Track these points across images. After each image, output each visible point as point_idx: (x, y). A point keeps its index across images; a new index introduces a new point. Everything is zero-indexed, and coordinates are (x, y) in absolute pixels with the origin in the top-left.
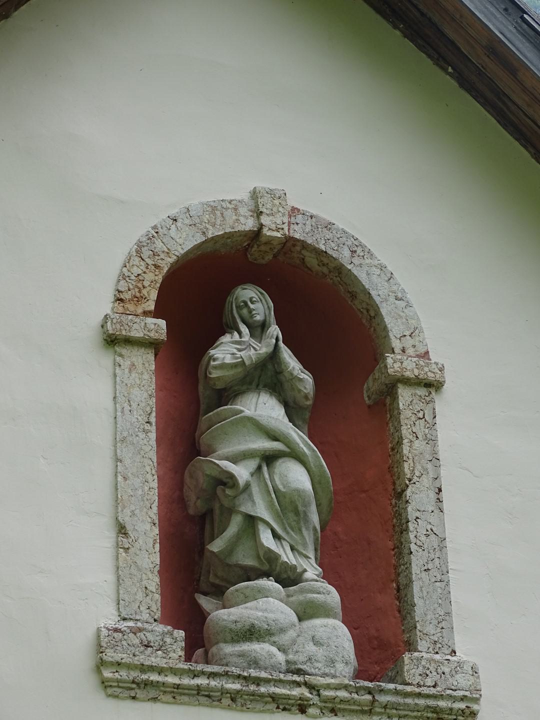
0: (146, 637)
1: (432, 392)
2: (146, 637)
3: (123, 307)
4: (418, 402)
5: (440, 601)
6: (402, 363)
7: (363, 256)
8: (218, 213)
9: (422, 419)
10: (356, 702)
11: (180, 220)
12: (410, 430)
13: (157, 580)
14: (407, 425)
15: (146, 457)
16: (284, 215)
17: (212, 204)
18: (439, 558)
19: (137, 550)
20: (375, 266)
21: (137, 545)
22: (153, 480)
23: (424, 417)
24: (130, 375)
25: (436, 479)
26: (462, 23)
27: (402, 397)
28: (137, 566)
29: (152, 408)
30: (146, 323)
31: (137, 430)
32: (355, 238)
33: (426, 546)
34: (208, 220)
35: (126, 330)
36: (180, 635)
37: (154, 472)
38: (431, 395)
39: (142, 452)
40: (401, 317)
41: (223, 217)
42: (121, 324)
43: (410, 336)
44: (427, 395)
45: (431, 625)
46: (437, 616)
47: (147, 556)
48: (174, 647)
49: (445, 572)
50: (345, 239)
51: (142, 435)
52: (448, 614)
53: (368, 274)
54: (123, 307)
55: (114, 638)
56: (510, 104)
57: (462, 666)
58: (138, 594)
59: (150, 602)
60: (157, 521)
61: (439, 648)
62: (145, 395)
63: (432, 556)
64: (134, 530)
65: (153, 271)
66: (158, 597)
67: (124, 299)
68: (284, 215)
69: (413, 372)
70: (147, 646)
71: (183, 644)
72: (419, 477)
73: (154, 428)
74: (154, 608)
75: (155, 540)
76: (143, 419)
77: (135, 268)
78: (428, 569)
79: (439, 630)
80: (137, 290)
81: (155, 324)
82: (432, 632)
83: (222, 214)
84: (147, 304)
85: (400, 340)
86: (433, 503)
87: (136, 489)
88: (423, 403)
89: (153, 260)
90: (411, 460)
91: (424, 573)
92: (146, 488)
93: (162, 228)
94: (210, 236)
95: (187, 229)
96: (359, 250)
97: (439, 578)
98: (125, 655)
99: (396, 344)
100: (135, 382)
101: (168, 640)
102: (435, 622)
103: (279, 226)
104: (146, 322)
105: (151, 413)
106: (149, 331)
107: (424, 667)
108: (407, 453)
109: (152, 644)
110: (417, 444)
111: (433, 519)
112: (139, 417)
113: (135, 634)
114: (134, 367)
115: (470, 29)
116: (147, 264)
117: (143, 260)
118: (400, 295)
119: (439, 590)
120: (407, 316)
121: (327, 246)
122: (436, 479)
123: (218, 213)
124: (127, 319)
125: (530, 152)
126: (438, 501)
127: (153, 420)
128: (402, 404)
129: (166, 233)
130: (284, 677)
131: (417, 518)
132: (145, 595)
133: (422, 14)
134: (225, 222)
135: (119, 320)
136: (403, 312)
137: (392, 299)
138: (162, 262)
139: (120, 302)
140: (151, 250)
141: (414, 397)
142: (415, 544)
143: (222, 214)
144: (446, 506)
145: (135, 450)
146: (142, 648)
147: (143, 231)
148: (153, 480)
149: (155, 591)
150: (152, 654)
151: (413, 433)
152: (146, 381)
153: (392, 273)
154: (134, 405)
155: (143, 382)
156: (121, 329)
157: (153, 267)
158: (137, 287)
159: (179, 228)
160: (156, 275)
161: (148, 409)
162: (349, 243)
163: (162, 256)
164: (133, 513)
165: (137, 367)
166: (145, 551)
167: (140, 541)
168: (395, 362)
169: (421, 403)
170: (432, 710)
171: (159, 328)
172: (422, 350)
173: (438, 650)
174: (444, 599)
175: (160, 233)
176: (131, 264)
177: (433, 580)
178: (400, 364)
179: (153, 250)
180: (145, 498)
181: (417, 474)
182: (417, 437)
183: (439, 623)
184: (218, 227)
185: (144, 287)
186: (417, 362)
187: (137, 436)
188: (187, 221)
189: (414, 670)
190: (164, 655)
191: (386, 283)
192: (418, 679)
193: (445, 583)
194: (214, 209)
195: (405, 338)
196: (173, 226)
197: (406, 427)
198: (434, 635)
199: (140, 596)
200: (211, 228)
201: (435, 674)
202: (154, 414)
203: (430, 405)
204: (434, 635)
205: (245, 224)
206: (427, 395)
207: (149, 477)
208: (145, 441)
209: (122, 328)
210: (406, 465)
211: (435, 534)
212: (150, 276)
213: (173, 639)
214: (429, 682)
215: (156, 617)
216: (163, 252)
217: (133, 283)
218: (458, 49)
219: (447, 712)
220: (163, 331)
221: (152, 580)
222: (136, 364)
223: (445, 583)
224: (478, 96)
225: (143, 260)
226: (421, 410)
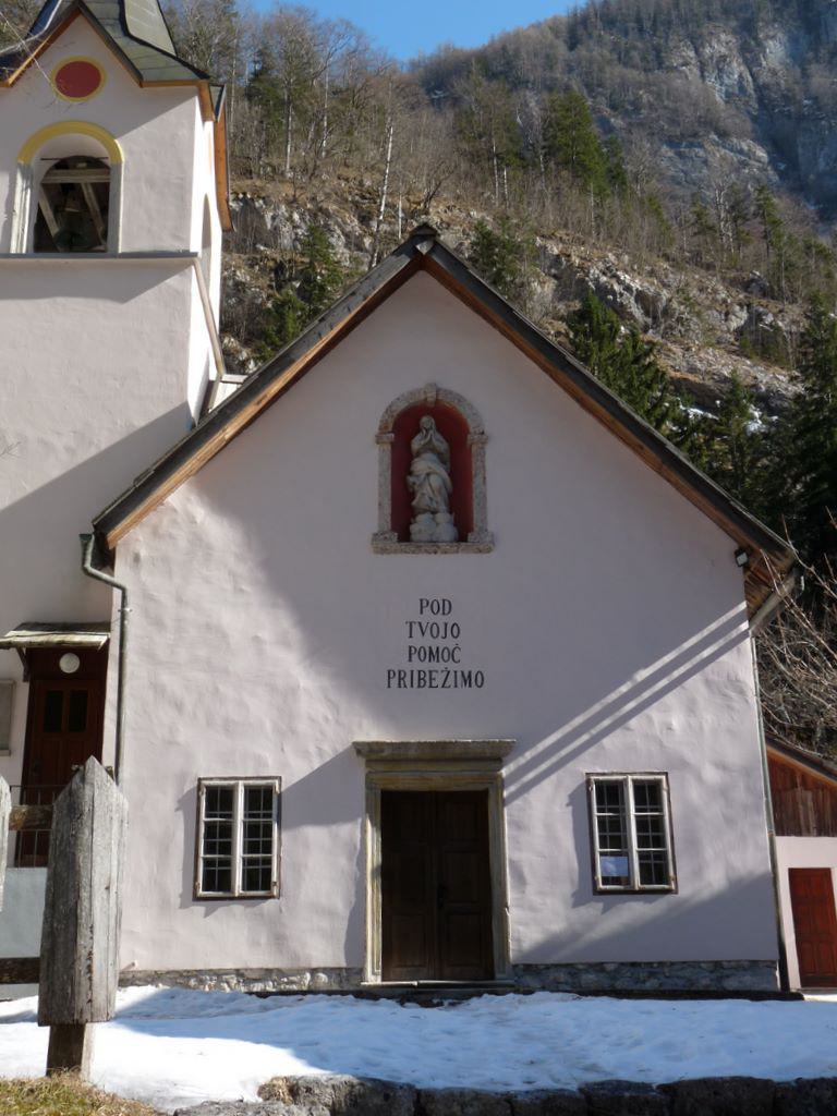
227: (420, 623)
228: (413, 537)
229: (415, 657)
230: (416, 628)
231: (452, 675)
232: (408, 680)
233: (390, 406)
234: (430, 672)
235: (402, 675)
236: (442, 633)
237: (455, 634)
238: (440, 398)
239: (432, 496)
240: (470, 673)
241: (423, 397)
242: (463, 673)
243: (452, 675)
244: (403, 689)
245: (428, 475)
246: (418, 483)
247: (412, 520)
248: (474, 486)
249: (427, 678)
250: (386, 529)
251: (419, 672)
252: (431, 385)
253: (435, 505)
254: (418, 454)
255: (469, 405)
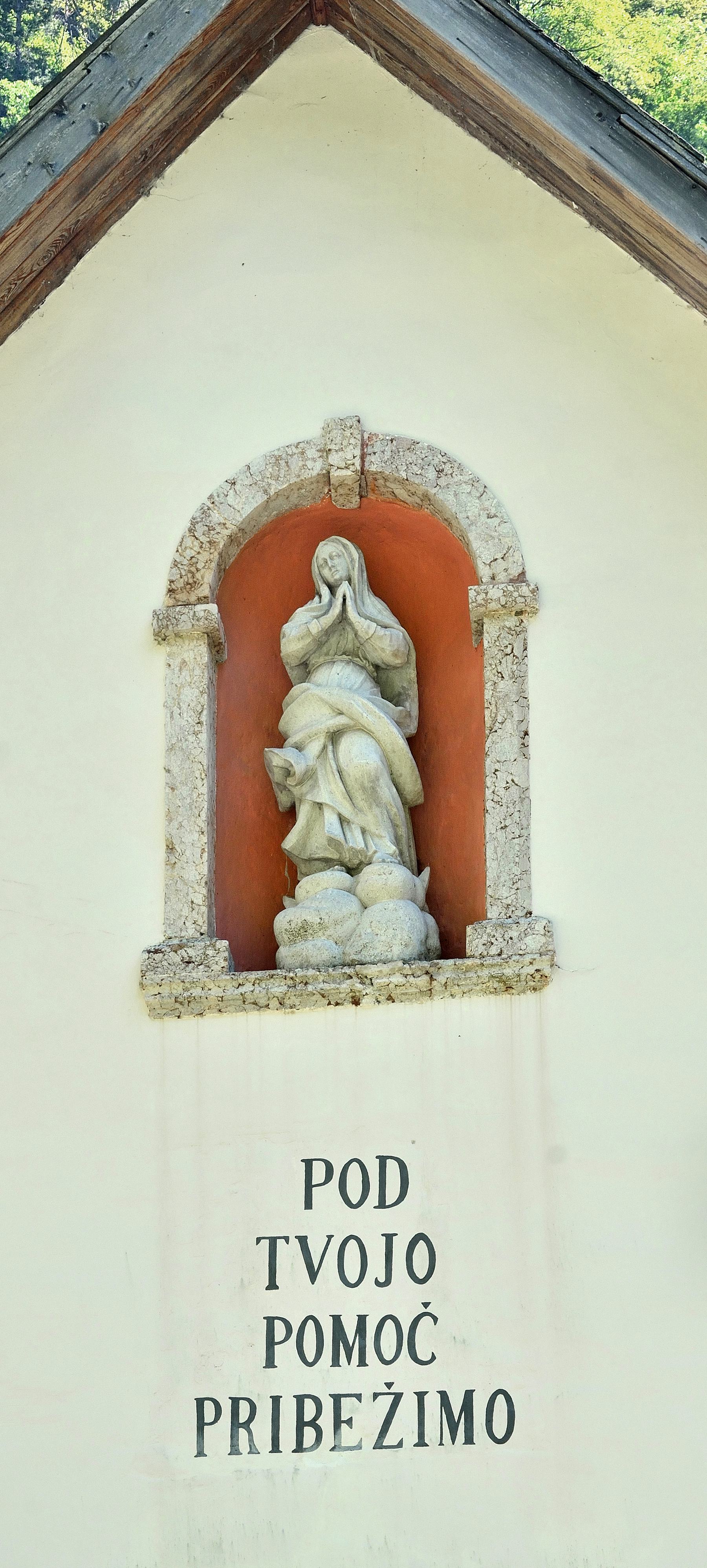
0: (188, 953)
1: (524, 620)
2: (188, 953)
3: (175, 598)
4: (507, 635)
5: (517, 860)
6: (486, 593)
7: (451, 474)
8: (282, 463)
9: (509, 655)
10: (412, 985)
11: (239, 482)
12: (494, 671)
13: (204, 891)
14: (491, 665)
15: (195, 761)
16: (355, 446)
17: (276, 453)
18: (519, 811)
19: (183, 863)
20: (465, 482)
21: (184, 858)
22: (203, 785)
23: (512, 652)
24: (181, 674)
25: (522, 721)
26: (559, 146)
27: (488, 633)
28: (183, 881)
29: (203, 706)
30: (195, 612)
31: (186, 733)
32: (443, 454)
33: (504, 801)
34: (271, 474)
35: (173, 624)
36: (223, 945)
37: (203, 776)
38: (523, 624)
39: (191, 757)
40: (493, 538)
41: (288, 466)
42: (167, 619)
43: (502, 558)
44: (518, 625)
45: (504, 888)
46: (512, 876)
47: (194, 868)
48: (217, 959)
49: (525, 826)
50: (430, 458)
51: (191, 738)
52: (526, 872)
53: (456, 495)
54: (175, 598)
55: (154, 960)
56: (633, 234)
57: (533, 927)
58: (183, 910)
59: (196, 916)
60: (205, 829)
61: (513, 911)
62: (196, 692)
63: (511, 810)
64: (182, 842)
65: (208, 549)
66: (204, 909)
67: (176, 589)
68: (355, 446)
69: (500, 601)
70: (189, 963)
71: (226, 954)
72: (502, 723)
73: (204, 728)
74: (200, 922)
75: (203, 849)
76: (193, 720)
77: (188, 551)
78: (506, 826)
79: (513, 891)
80: (190, 575)
81: (205, 610)
82: (505, 895)
83: (287, 463)
84: (202, 588)
85: (490, 565)
86: (516, 750)
87: (184, 798)
88: (512, 635)
89: (207, 536)
90: (493, 706)
91: (499, 833)
92: (195, 795)
93: (218, 496)
94: (272, 492)
95: (247, 490)
96: (447, 468)
97: (517, 833)
98: (166, 975)
99: (484, 572)
100: (186, 680)
101: (210, 952)
102: (510, 883)
103: (349, 462)
104: (195, 610)
105: (202, 711)
106: (198, 620)
107: (489, 935)
108: (490, 697)
109: (193, 960)
110: (502, 685)
111: (515, 769)
112: (190, 719)
113: (176, 952)
114: (185, 664)
115: (568, 152)
116: (201, 542)
117: (197, 539)
118: (493, 511)
119: (517, 848)
120: (500, 535)
121: (409, 471)
122: (522, 721)
123: (282, 463)
124: (175, 611)
125: (672, 288)
126: (523, 746)
127: (204, 718)
128: (487, 642)
129: (223, 501)
130: (333, 970)
131: (496, 770)
132: (191, 909)
133: (528, 145)
134: (290, 471)
135: (165, 616)
136: (496, 531)
137: (484, 518)
138: (218, 537)
139: (171, 593)
140: (206, 526)
141: (501, 632)
142: (492, 800)
143: (287, 463)
144: (532, 750)
145: (184, 756)
146: (183, 965)
147: (198, 505)
148: (203, 785)
149: (201, 904)
150: (194, 970)
151: (498, 673)
152: (198, 677)
153: (485, 487)
154: (184, 707)
155: (194, 679)
156: (167, 625)
157: (208, 544)
158: (190, 572)
159: (238, 493)
160: (211, 554)
161: (199, 708)
162: (436, 461)
163: (218, 529)
164: (181, 825)
165: (188, 663)
166: (192, 863)
167: (188, 853)
168: (478, 593)
169: (510, 637)
170: (498, 979)
171: (209, 614)
172: (515, 572)
173: (510, 914)
174: (521, 856)
175: (216, 503)
176: (183, 547)
177: (512, 836)
178: (484, 594)
179: (208, 524)
180: (193, 807)
181: (500, 719)
182: (502, 677)
183: (514, 883)
184: (282, 479)
185: (198, 570)
186: (505, 589)
187: (186, 740)
188: (248, 482)
189: (477, 940)
190: (206, 969)
191: (477, 501)
192: (481, 949)
193: (524, 838)
194: (278, 459)
195: (496, 562)
196: (231, 491)
197: (489, 668)
198: (507, 898)
199: (186, 911)
200: (273, 482)
201: (502, 940)
202: (205, 712)
203: (521, 636)
204: (507, 898)
205: (312, 469)
206: (518, 625)
207: (199, 783)
208: (195, 745)
209: (168, 623)
210: (487, 713)
211: (517, 785)
212: (204, 557)
213: (216, 950)
214: (494, 950)
215: (202, 931)
216: (219, 524)
217: (186, 568)
218: (569, 178)
219: (515, 979)
220: (213, 617)
221: (199, 893)
222: (187, 660)
223: (524, 838)
224: (608, 231)
225: (197, 539)
226: (510, 644)
227: (303, 1241)
228: (283, 953)
229: (286, 1352)
230: (289, 1254)
231: (408, 1408)
232: (262, 1427)
233: (205, 511)
234: (337, 1399)
235: (243, 1416)
236: (376, 1269)
237: (500, 1433)
238: (374, 465)
239: (347, 811)
240: (469, 1396)
241: (316, 468)
242: (444, 1395)
243: (408, 1408)
244: (244, 1458)
245: (334, 737)
246: (299, 769)
247: (287, 901)
248: (489, 764)
249: (326, 1421)
250: (191, 931)
251: (300, 1400)
252: (342, 423)
253: (356, 841)
254: (306, 668)
255: (475, 481)
